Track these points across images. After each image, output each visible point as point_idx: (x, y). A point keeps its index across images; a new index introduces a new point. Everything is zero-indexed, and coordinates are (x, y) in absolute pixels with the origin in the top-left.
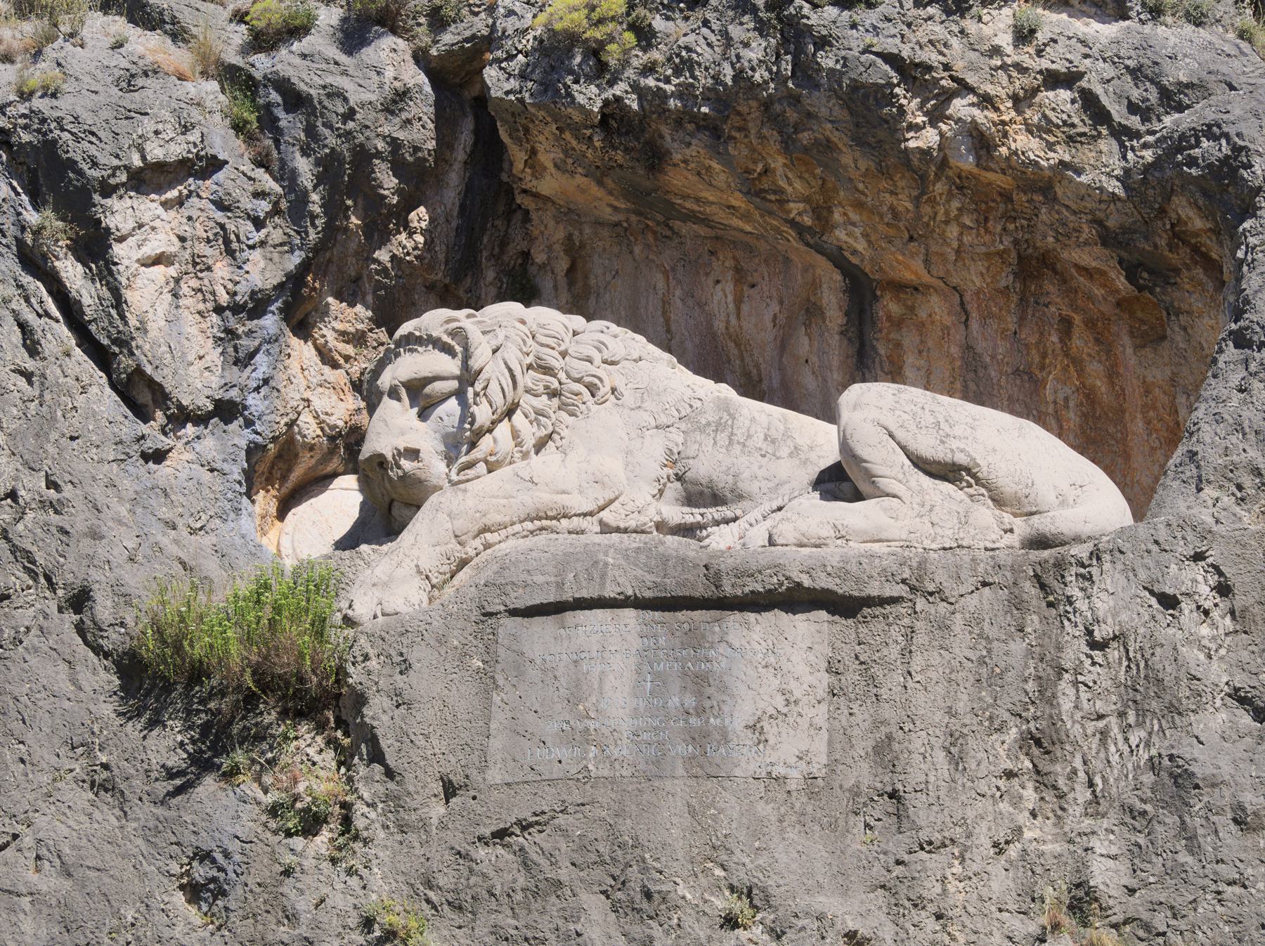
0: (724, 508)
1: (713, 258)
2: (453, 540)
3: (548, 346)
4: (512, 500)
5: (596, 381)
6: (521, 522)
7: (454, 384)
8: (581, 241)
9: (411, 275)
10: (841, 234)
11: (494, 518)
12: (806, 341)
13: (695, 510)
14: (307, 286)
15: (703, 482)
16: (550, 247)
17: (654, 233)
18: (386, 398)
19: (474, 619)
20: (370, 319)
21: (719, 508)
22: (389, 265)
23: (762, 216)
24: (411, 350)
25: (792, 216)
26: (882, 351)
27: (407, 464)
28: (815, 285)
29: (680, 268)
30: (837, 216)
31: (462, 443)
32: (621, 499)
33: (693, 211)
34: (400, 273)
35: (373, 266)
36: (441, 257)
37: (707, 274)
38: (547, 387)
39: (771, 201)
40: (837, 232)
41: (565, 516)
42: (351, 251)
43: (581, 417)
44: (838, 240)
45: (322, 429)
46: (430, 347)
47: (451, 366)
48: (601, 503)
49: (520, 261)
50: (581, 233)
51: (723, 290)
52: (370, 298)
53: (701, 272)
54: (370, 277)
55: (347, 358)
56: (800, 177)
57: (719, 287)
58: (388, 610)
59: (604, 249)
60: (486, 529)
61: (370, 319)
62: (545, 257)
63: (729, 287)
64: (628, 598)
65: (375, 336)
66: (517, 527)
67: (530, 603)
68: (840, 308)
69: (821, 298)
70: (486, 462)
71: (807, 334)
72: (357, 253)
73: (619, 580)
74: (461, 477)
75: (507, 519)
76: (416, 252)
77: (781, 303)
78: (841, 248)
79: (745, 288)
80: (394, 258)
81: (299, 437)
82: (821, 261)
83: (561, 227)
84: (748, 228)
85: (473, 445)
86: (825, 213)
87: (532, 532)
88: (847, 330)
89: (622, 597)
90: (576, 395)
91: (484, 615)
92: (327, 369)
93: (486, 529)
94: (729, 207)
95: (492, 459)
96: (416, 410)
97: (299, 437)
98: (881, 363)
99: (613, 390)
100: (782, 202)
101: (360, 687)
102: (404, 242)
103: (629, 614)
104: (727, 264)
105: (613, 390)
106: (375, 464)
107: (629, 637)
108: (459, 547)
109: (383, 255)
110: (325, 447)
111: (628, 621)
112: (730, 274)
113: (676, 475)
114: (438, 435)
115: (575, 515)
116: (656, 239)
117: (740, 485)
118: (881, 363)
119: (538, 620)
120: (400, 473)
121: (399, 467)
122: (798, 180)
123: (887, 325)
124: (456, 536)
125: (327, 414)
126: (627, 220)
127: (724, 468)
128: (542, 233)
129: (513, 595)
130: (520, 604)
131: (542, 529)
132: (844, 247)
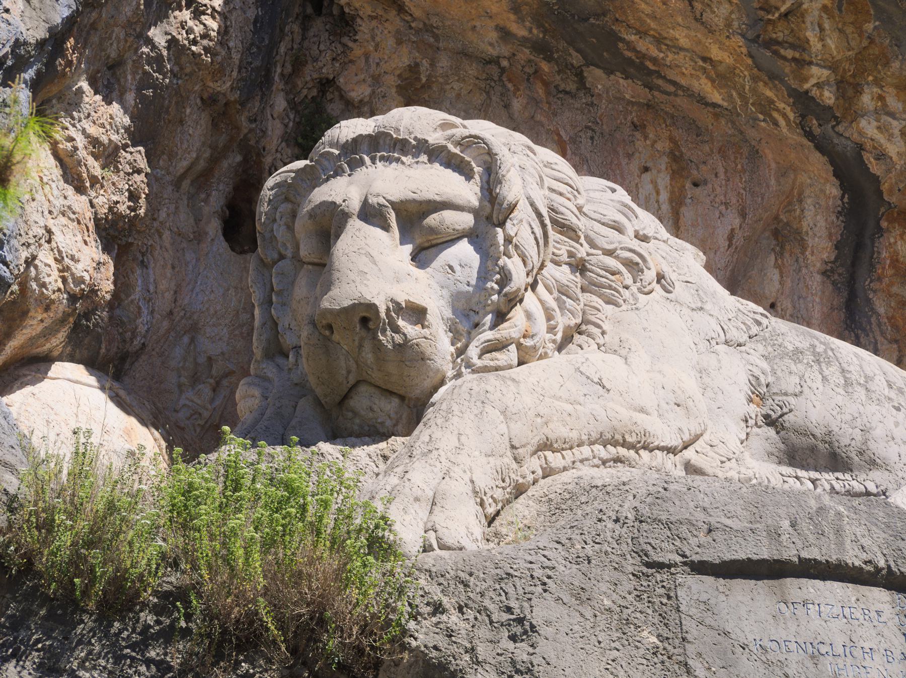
0: (847, 476)
1: (638, 135)
2: (509, 454)
3: (561, 194)
4: (578, 407)
5: (637, 259)
6: (592, 443)
7: (466, 220)
8: (429, 77)
9: (190, 75)
10: (869, 128)
11: (559, 431)
12: (775, 275)
13: (801, 473)
14: (64, 56)
15: (817, 432)
16: (376, 80)
17: (546, 84)
18: (355, 225)
19: (630, 569)
20: (127, 130)
21: (840, 475)
22: (165, 53)
23: (755, 79)
24: (386, 159)
25: (806, 86)
26: (881, 308)
27: (411, 330)
28: (793, 199)
29: (584, 138)
30: (867, 100)
31: (485, 306)
32: (706, 437)
33: (643, 56)
34: (176, 69)
35: (145, 50)
36: (236, 57)
37: (630, 156)
38: (571, 255)
39: (785, 58)
40: (863, 123)
41: (645, 448)
42: (122, 19)
43: (624, 307)
44: (861, 133)
45: (64, 280)
46: (424, 158)
47: (467, 191)
48: (686, 437)
49: (314, 92)
50: (433, 65)
51: (654, 183)
52: (130, 97)
53: (620, 151)
54: (137, 64)
55: (94, 180)
56: (841, 31)
57: (647, 177)
58: (449, 541)
59: (458, 96)
60: (546, 446)
61: (127, 130)
62: (368, 91)
63: (664, 180)
64: (878, 570)
65: (128, 156)
66: (586, 451)
67: (728, 557)
68: (830, 236)
69: (800, 219)
70: (519, 346)
71: (777, 266)
72: (129, 24)
73: (863, 541)
74: (487, 361)
75: (574, 435)
76: (205, 42)
77: (743, 215)
78: (860, 147)
79: (688, 185)
80: (172, 42)
81: (34, 286)
82: (818, 164)
83: (405, 50)
84: (716, 97)
85: (501, 317)
86: (850, 92)
87: (604, 462)
88: (832, 271)
89: (870, 568)
90: (613, 274)
91: (649, 565)
92: (70, 191)
93: (546, 446)
94: (705, 59)
95: (528, 343)
96: (409, 248)
97: (34, 286)
98: (879, 325)
99: (660, 277)
100: (801, 63)
101: (434, 654)
102: (191, 23)
103: (879, 597)
104: (659, 146)
105: (660, 277)
106: (357, 319)
107: (886, 632)
108: (514, 465)
109: (157, 35)
110: (61, 308)
111: (880, 607)
112: (663, 162)
113: (766, 417)
114: (445, 292)
115: (658, 448)
116: (548, 93)
117: (872, 445)
118: (879, 325)
119: (739, 585)
120: (398, 338)
121: (396, 330)
122: (836, 35)
123: (890, 272)
124: (513, 447)
125: (73, 258)
126: (512, 57)
127: (848, 417)
128: (367, 56)
129: (693, 541)
130: (711, 556)
131: (618, 460)
132: (868, 146)
